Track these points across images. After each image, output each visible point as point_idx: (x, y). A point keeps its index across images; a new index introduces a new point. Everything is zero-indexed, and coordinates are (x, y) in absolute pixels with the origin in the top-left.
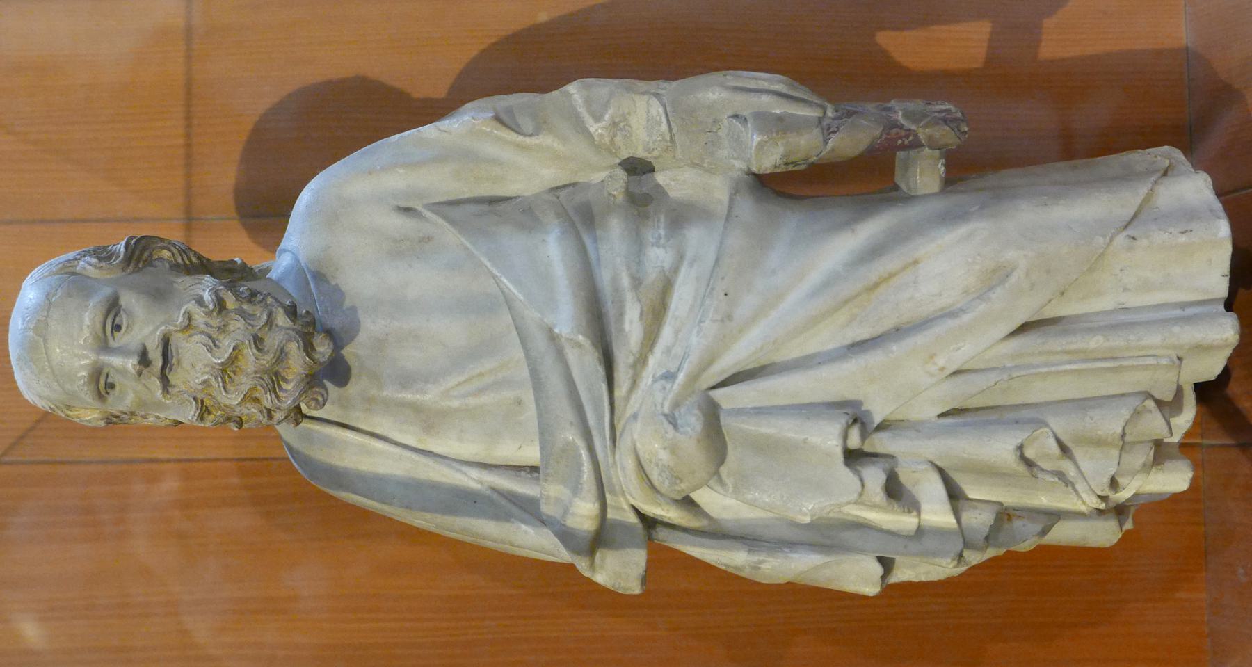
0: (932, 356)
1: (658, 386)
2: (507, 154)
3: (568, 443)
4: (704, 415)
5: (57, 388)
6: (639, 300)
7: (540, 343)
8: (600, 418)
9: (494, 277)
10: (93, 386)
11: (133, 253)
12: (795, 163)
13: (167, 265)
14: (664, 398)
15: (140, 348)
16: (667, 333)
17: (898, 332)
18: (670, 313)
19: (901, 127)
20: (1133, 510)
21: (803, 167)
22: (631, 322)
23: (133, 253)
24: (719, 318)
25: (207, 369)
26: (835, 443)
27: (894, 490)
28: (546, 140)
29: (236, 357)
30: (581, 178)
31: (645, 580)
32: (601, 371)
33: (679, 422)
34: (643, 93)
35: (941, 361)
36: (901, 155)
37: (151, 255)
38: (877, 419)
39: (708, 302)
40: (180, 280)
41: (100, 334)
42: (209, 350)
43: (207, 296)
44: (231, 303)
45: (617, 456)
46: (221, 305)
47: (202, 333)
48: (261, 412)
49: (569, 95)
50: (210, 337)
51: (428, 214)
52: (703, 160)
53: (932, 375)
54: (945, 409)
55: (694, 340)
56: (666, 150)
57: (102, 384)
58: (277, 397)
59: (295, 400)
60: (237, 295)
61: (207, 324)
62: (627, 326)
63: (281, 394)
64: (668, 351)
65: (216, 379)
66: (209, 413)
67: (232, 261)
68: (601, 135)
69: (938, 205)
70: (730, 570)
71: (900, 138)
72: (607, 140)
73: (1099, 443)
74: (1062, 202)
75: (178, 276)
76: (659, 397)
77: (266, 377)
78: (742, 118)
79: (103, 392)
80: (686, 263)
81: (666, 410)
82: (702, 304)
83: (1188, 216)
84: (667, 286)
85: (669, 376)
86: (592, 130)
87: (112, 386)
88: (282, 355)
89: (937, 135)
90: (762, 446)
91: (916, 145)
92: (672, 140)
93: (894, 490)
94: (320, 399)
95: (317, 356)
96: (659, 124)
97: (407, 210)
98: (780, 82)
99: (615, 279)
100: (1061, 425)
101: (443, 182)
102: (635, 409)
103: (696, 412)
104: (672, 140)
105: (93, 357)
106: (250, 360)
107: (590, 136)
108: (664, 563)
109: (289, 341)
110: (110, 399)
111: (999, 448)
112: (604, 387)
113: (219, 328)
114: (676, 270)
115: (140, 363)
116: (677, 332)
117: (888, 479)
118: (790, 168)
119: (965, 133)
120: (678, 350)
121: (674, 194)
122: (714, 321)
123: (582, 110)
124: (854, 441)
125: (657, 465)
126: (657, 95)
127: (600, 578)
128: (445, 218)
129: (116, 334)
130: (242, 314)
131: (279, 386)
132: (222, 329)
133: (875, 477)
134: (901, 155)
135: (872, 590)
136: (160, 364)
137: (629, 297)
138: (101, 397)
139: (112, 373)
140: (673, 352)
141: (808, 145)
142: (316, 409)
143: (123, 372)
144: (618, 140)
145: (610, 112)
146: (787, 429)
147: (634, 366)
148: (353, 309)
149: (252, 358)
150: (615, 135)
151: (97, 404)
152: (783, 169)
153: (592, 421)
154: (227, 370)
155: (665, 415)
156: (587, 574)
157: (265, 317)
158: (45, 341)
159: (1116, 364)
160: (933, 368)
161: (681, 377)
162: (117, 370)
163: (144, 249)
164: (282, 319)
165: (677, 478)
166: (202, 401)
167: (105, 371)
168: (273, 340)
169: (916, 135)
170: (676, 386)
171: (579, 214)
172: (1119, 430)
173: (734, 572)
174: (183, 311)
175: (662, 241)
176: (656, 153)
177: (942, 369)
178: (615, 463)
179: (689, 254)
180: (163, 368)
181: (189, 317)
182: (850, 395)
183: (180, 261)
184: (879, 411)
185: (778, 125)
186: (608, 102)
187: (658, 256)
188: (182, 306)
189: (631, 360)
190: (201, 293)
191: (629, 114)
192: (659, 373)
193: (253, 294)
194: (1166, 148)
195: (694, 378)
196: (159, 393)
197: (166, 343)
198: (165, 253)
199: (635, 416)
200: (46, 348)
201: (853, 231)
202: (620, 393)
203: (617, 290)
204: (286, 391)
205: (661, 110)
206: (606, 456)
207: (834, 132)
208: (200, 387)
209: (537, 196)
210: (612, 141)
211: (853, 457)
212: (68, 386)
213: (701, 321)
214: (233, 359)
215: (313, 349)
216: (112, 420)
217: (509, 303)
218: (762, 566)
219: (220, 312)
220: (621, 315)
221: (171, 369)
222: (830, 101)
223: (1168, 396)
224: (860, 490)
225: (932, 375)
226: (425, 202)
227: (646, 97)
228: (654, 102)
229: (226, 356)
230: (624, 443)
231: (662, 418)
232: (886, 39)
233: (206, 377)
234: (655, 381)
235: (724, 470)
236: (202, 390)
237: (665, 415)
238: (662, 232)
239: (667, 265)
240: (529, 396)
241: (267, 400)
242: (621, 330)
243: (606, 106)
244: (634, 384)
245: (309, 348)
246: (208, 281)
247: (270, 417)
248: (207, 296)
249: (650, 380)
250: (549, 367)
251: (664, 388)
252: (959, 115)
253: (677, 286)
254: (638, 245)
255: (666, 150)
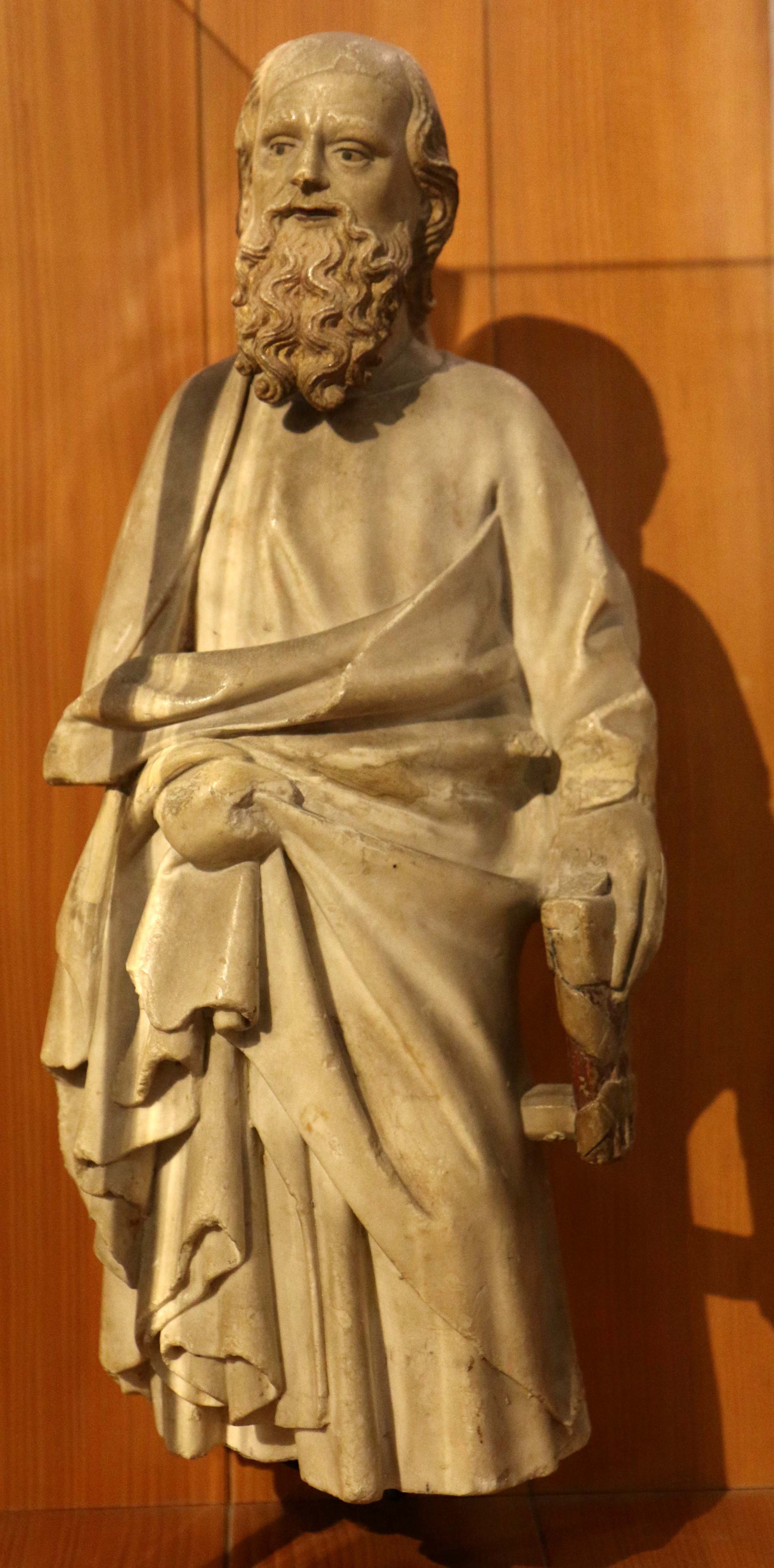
0: (323, 1114)
1: (286, 786)
2: (564, 618)
3: (218, 681)
4: (252, 841)
5: (277, 88)
6: (387, 764)
7: (335, 649)
8: (248, 719)
9: (414, 597)
10: (280, 129)
11: (437, 176)
12: (554, 953)
13: (424, 217)
14: (270, 793)
15: (325, 182)
16: (348, 798)
17: (351, 1077)
18: (374, 803)
19: (601, 1081)
20: (145, 1391)
21: (550, 964)
22: (361, 755)
23: (437, 176)
24: (367, 858)
25: (300, 260)
26: (220, 995)
27: (165, 1074)
28: (580, 662)
29: (315, 295)
30: (536, 708)
31: (60, 782)
32: (301, 717)
33: (244, 810)
34: (637, 776)
35: (319, 1126)
36: (570, 1088)
37: (436, 197)
38: (249, 1052)
39: (385, 845)
40: (406, 230)
41: (339, 135)
42: (323, 263)
43: (386, 260)
44: (380, 288)
45: (202, 740)
46: (376, 276)
47: (343, 255)
48: (253, 326)
49: (635, 689)
50: (339, 263)
51: (489, 522)
52: (558, 847)
53: (302, 1115)
54: (262, 1135)
55: (341, 828)
56: (570, 805)
57: (281, 139)
58: (269, 344)
59: (266, 364)
60: (388, 297)
61: (353, 260)
62: (355, 750)
63: (272, 348)
64: (328, 799)
65: (290, 272)
66: (251, 267)
67: (430, 296)
68: (585, 726)
69: (507, 1128)
70: (72, 884)
71: (587, 1080)
72: (580, 733)
73: (223, 1327)
74: (513, 1280)
75: (410, 228)
76: (271, 786)
77: (292, 330)
78: (586, 850)
79: (274, 141)
80: (434, 824)
81: (257, 795)
82: (383, 840)
83: (498, 1436)
84: (406, 799)
85: (298, 800)
86: (592, 715)
87: (280, 151)
88: (319, 348)
89: (591, 1125)
90: (216, 909)
91: (580, 1100)
92: (580, 812)
93: (165, 1074)
94: (269, 394)
95: (318, 389)
96: (600, 794)
97: (491, 501)
98: (653, 936)
99: (411, 738)
100: (241, 1282)
101: (528, 541)
102: (259, 760)
103: (256, 830)
104: (580, 812)
105: (313, 127)
106: (312, 310)
107: (584, 713)
108: (83, 800)
109: (335, 355)
110: (264, 151)
111: (214, 1201)
112: (284, 722)
113: (349, 274)
114: (424, 810)
115: (306, 182)
116: (350, 810)
117: (178, 1063)
118: (549, 948)
119: (596, 1160)
120: (328, 810)
121: (520, 816)
122: (363, 850)
123: (618, 704)
124: (222, 1020)
125: (192, 785)
126: (634, 793)
127: (62, 730)
128: (484, 542)
129: (340, 154)
130: (368, 299)
131: (283, 346)
132: (349, 278)
133: (177, 1047)
134: (570, 1088)
135: (48, 1056)
136: (306, 206)
137: (392, 753)
138: (267, 139)
139: (295, 150)
140: (327, 806)
141: (572, 964)
142: (256, 390)
143: (296, 164)
144: (581, 747)
145: (615, 737)
146: (234, 940)
147: (310, 758)
148: (374, 434)
149: (314, 313)
150: (586, 742)
151: (259, 135)
152: (548, 939)
153: (245, 710)
154: (297, 283)
155: (251, 794)
156: (67, 713)
157: (363, 327)
158: (330, 72)
159: (317, 1347)
160: (310, 1117)
161: (295, 812)
162: (298, 157)
163: (440, 188)
164: (361, 347)
165: (178, 810)
166: (264, 258)
167: (298, 143)
168: (336, 337)
169: (590, 1099)
170: (284, 807)
171: (492, 696)
172: (238, 1352)
173: (74, 875)
174: (369, 231)
175: (460, 797)
176: (566, 792)
177: (309, 1128)
178: (195, 737)
179: (446, 829)
180: (301, 210)
181: (361, 239)
182: (277, 1017)
183: (428, 240)
184: (259, 1054)
185: (357, 350)
186: (626, 735)
187: (441, 791)
188: (375, 231)
189: (317, 754)
190: (390, 254)
191: (612, 759)
192: (302, 789)
193: (391, 316)
194: (587, 1428)
195: (296, 828)
196: (273, 207)
197: (330, 212)
198: (437, 214)
199: (250, 759)
200: (322, 72)
201: (476, 1024)
202: (278, 742)
203: (399, 740)
204: (277, 353)
205: (617, 796)
206: (205, 726)
207: (592, 999)
208: (280, 253)
209: (514, 654)
210: (580, 739)
211: (201, 1021)
212: (279, 100)
213: (362, 837)
214: (312, 290)
215: (325, 386)
216: (245, 153)
217: (382, 614)
218: (76, 922)
219: (368, 275)
220: (369, 743)
221: (299, 219)
222: (631, 993)
223: (282, 1419)
224: (165, 1028)
225: (302, 1115)
226: (506, 527)
227: (632, 779)
228: (627, 789)
229: (316, 283)
230: (217, 746)
231: (248, 790)
232: (724, 1108)
233: (291, 260)
234: (292, 783)
235: (188, 868)
236: (277, 256)
237: (251, 794)
238: (471, 798)
239: (430, 800)
240: (275, 637)
241: (266, 333)
242: (352, 744)
243: (618, 732)
244: (288, 759)
245: (326, 379)
246: (405, 264)
247: (247, 337)
248: (386, 260)
249: (293, 778)
250: (310, 659)
251: (283, 793)
252: (617, 1154)
253: (405, 811)
254: (457, 767)
255: (570, 805)
